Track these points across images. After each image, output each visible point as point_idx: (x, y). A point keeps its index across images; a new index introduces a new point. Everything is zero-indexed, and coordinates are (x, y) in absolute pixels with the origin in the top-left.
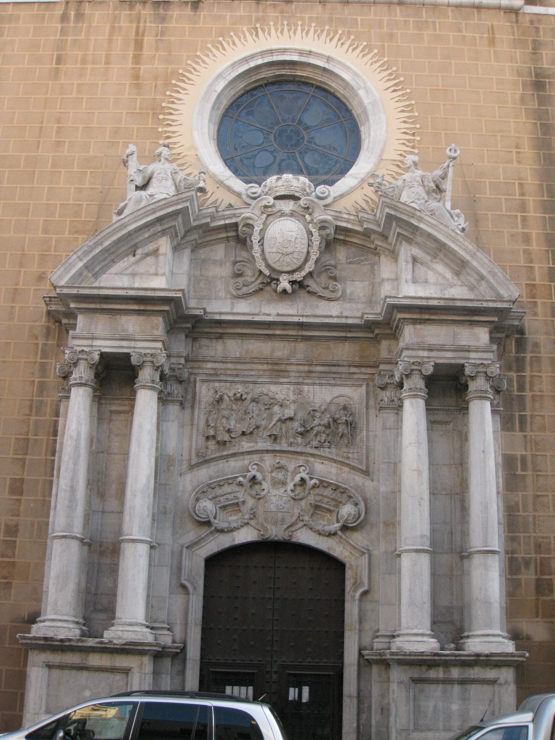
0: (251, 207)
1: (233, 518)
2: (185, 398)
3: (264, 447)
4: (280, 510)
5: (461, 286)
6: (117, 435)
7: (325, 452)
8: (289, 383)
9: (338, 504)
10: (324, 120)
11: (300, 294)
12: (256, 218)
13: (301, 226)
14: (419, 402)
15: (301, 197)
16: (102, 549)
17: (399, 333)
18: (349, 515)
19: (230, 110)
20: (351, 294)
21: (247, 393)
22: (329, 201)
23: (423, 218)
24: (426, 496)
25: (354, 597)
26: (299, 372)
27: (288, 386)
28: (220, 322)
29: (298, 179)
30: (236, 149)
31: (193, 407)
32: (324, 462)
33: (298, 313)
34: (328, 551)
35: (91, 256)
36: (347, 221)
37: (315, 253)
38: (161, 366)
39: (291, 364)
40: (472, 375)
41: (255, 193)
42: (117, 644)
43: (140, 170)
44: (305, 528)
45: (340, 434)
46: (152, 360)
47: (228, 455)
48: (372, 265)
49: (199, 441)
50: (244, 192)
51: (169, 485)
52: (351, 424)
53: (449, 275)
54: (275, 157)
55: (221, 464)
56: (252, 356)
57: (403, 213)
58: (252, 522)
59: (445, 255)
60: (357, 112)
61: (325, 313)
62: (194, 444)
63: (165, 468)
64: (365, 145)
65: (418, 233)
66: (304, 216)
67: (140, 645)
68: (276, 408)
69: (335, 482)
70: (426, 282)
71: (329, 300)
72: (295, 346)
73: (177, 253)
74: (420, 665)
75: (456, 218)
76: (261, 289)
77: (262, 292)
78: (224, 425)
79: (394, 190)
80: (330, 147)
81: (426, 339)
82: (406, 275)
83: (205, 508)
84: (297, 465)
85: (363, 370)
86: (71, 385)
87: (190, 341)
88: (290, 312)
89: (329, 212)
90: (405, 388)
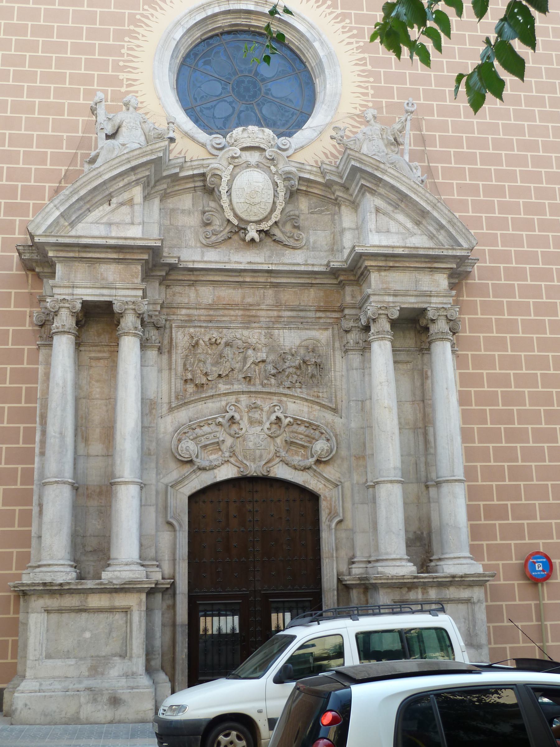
0: (219, 158)
1: (213, 457)
2: (162, 344)
3: (239, 388)
4: (259, 448)
5: (421, 235)
6: (97, 381)
7: (298, 392)
8: (261, 328)
9: (312, 440)
10: (280, 72)
11: (266, 243)
12: (224, 169)
13: (267, 177)
14: (386, 344)
15: (266, 148)
16: (90, 491)
17: (362, 280)
18: (323, 450)
19: (188, 59)
20: (315, 243)
21: (221, 338)
22: (290, 152)
23: (386, 171)
24: (397, 431)
25: (329, 526)
26: (269, 317)
27: (260, 331)
28: (192, 270)
29: (263, 131)
30: (196, 99)
31: (170, 352)
32: (296, 401)
33: (265, 261)
34: (303, 484)
35: (67, 205)
36: (310, 172)
37: (281, 204)
38: (143, 314)
39: (261, 309)
40: (434, 318)
41: (219, 144)
42: (117, 585)
43: (109, 119)
44: (281, 463)
45: (310, 375)
46: (134, 307)
47: (206, 397)
48: (333, 215)
49: (178, 385)
50: (208, 143)
51: (152, 427)
52: (319, 365)
53: (409, 224)
54: (234, 108)
55: (200, 406)
56: (224, 303)
57: (368, 166)
58: (232, 460)
59: (407, 206)
60: (312, 63)
61: (290, 261)
62: (173, 388)
63: (148, 411)
64: (320, 97)
65: (381, 185)
66: (270, 167)
67: (139, 584)
68: (250, 352)
69: (308, 420)
70: (388, 231)
71: (294, 248)
72: (264, 292)
73: (147, 202)
74: (401, 588)
75: (415, 171)
76: (230, 238)
77: (230, 240)
78: (202, 369)
79: (355, 143)
80: (287, 99)
81: (390, 285)
82: (371, 224)
83: (188, 448)
84: (272, 405)
85: (328, 314)
86: (53, 333)
87: (163, 288)
88: (258, 260)
89: (293, 164)
90: (372, 331)
